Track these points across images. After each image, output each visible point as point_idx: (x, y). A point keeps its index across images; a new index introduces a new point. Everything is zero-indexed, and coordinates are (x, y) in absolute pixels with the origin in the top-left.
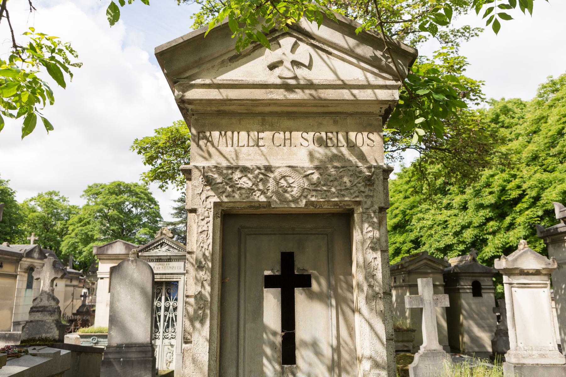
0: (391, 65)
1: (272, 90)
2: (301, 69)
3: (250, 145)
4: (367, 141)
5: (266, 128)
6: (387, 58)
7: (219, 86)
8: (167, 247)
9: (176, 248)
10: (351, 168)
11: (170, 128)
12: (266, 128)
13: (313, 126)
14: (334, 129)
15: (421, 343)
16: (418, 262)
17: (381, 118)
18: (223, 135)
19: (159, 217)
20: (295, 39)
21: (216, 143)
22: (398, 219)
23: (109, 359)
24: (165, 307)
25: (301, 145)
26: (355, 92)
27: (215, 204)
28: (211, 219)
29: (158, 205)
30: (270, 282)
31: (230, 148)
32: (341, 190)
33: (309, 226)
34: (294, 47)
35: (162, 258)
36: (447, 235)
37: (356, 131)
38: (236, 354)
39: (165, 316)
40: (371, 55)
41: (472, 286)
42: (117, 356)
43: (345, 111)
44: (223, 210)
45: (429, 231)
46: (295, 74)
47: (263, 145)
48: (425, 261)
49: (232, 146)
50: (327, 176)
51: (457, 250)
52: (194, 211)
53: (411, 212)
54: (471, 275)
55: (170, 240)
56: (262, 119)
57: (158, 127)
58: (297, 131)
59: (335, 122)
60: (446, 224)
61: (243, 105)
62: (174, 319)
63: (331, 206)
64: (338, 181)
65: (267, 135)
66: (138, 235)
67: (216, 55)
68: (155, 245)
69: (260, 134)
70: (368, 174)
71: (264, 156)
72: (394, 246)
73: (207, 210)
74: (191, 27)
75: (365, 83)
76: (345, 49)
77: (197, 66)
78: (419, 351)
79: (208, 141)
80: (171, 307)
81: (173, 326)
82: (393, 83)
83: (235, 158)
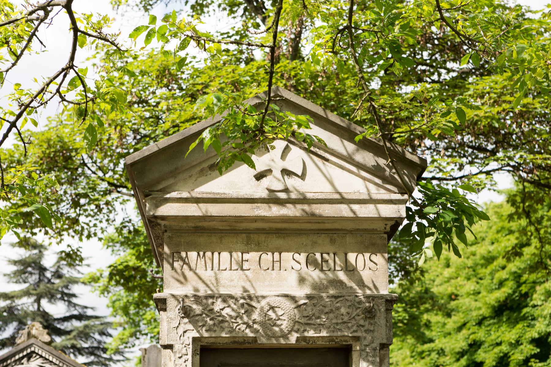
0: (396, 176)
1: (259, 205)
2: (293, 179)
3: (233, 268)
4: (369, 264)
5: (251, 248)
6: (391, 169)
7: (197, 201)
8: (40, 361)
10: (349, 298)
11: (46, 135)
12: (251, 248)
13: (306, 245)
14: (331, 249)
17: (386, 236)
18: (201, 256)
20: (286, 143)
21: (193, 265)
22: (506, 290)
25: (292, 268)
26: (355, 207)
27: (194, 339)
28: (190, 357)
31: (209, 273)
32: (337, 324)
33: (301, 363)
34: (286, 151)
37: (356, 252)
40: (373, 164)
43: (343, 228)
44: (201, 346)
46: (286, 185)
47: (248, 268)
49: (212, 270)
50: (321, 307)
52: (169, 347)
53: (533, 277)
55: (46, 347)
56: (247, 237)
58: (288, 252)
61: (225, 221)
63: (325, 342)
64: (334, 313)
65: (253, 256)
67: (194, 163)
68: (17, 357)
69: (244, 255)
71: (250, 281)
72: (497, 350)
73: (185, 347)
75: (366, 197)
76: (344, 156)
77: (172, 177)
79: (185, 263)
82: (398, 197)
83: (215, 284)
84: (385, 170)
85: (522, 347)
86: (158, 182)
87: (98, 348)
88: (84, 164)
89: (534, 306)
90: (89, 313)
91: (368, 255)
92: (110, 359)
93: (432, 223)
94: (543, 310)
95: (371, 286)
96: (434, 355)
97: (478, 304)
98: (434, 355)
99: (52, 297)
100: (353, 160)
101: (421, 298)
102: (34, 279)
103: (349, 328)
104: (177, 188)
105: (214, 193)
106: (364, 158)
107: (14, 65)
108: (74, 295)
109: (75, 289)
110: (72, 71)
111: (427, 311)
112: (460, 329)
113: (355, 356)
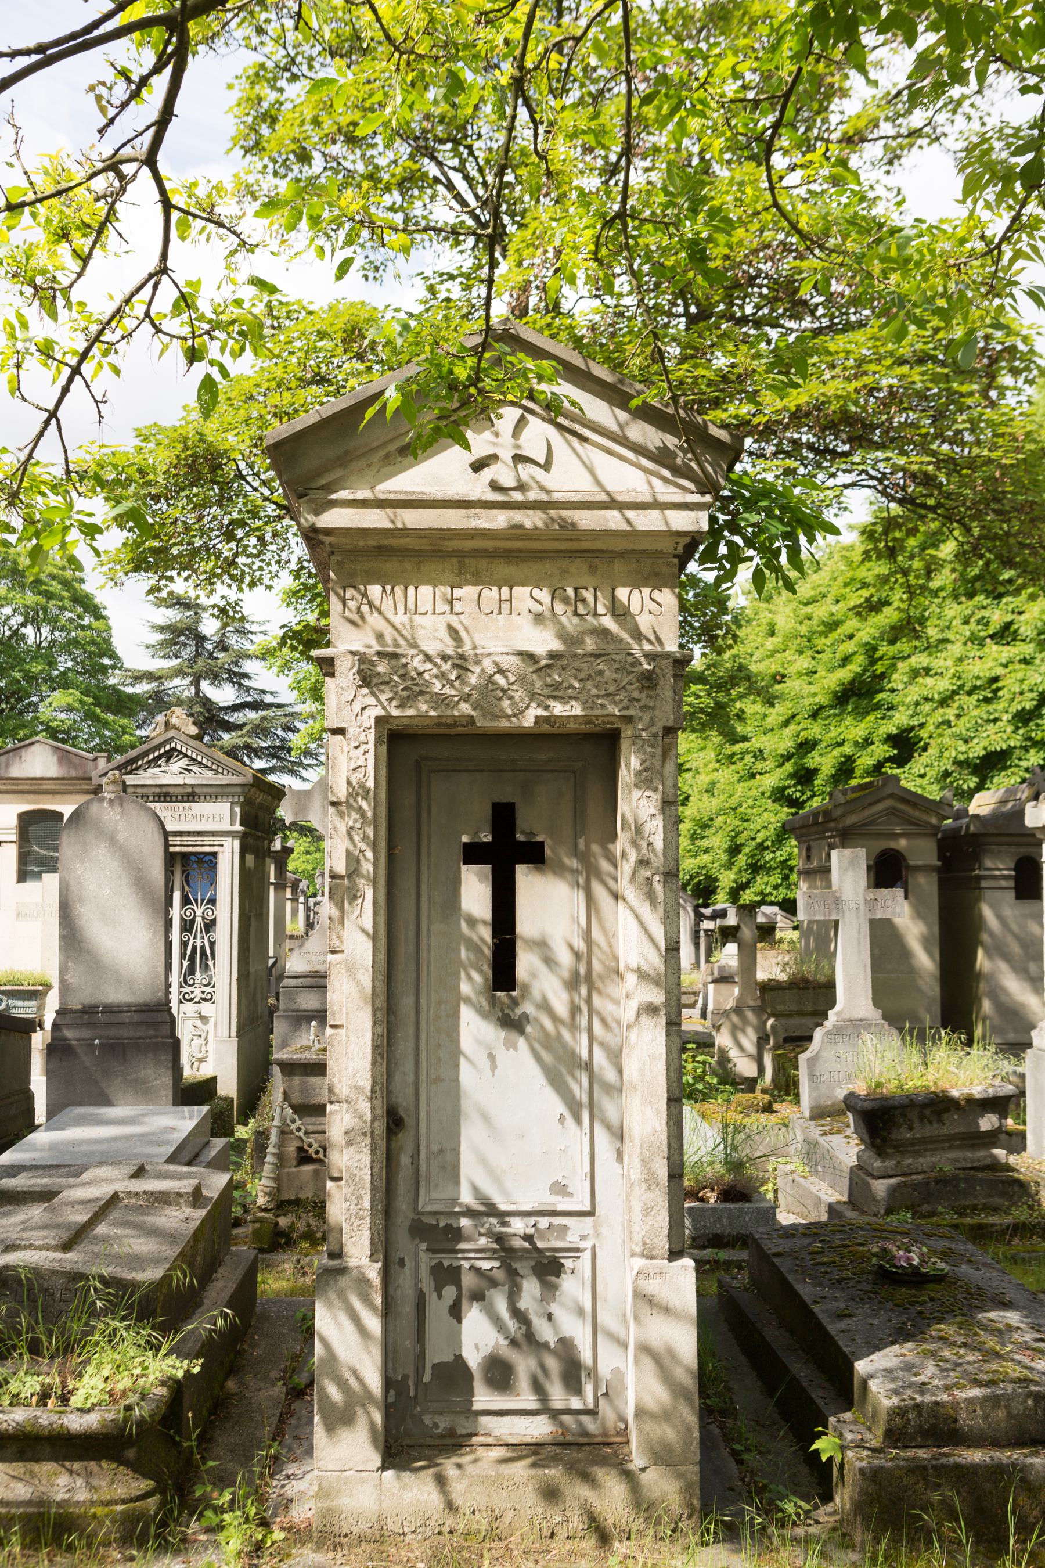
1: (478, 511)
4: (650, 605)
6: (685, 452)
8: (184, 762)
9: (209, 764)
10: (617, 658)
13: (551, 576)
15: (832, 1004)
16: (871, 804)
17: (676, 561)
19: (111, 657)
20: (520, 412)
22: (854, 668)
23: (66, 1039)
24: (182, 919)
26: (630, 514)
27: (378, 720)
28: (371, 746)
29: (104, 618)
30: (473, 854)
32: (598, 697)
33: (543, 757)
35: (171, 790)
36: (995, 720)
38: (414, 975)
39: (184, 944)
41: (1015, 870)
42: (85, 1033)
45: (941, 711)
48: (888, 803)
51: (1017, 766)
52: (340, 731)
54: (1016, 839)
55: (193, 743)
57: (144, 421)
59: (593, 570)
60: (994, 687)
62: (208, 952)
65: (467, 592)
66: (45, 712)
67: (375, 444)
68: (151, 757)
70: (647, 667)
72: (837, 752)
74: (230, 110)
75: (648, 498)
78: (826, 1023)
80: (199, 920)
81: (206, 968)
82: (696, 498)
84: (676, 456)
85: (873, 747)
86: (320, 473)
87: (282, 748)
88: (240, 476)
89: (893, 691)
90: (268, 699)
91: (648, 590)
92: (300, 764)
93: (749, 543)
94: (906, 696)
95: (652, 638)
96: (749, 759)
97: (813, 689)
98: (749, 759)
99: (215, 678)
100: (627, 438)
101: (732, 678)
102: (188, 652)
103: (615, 703)
104: (348, 483)
105: (406, 493)
106: (644, 434)
107: (80, 275)
108: (246, 676)
109: (249, 666)
110: (165, 277)
111: (741, 697)
112: (786, 723)
113: (625, 745)
